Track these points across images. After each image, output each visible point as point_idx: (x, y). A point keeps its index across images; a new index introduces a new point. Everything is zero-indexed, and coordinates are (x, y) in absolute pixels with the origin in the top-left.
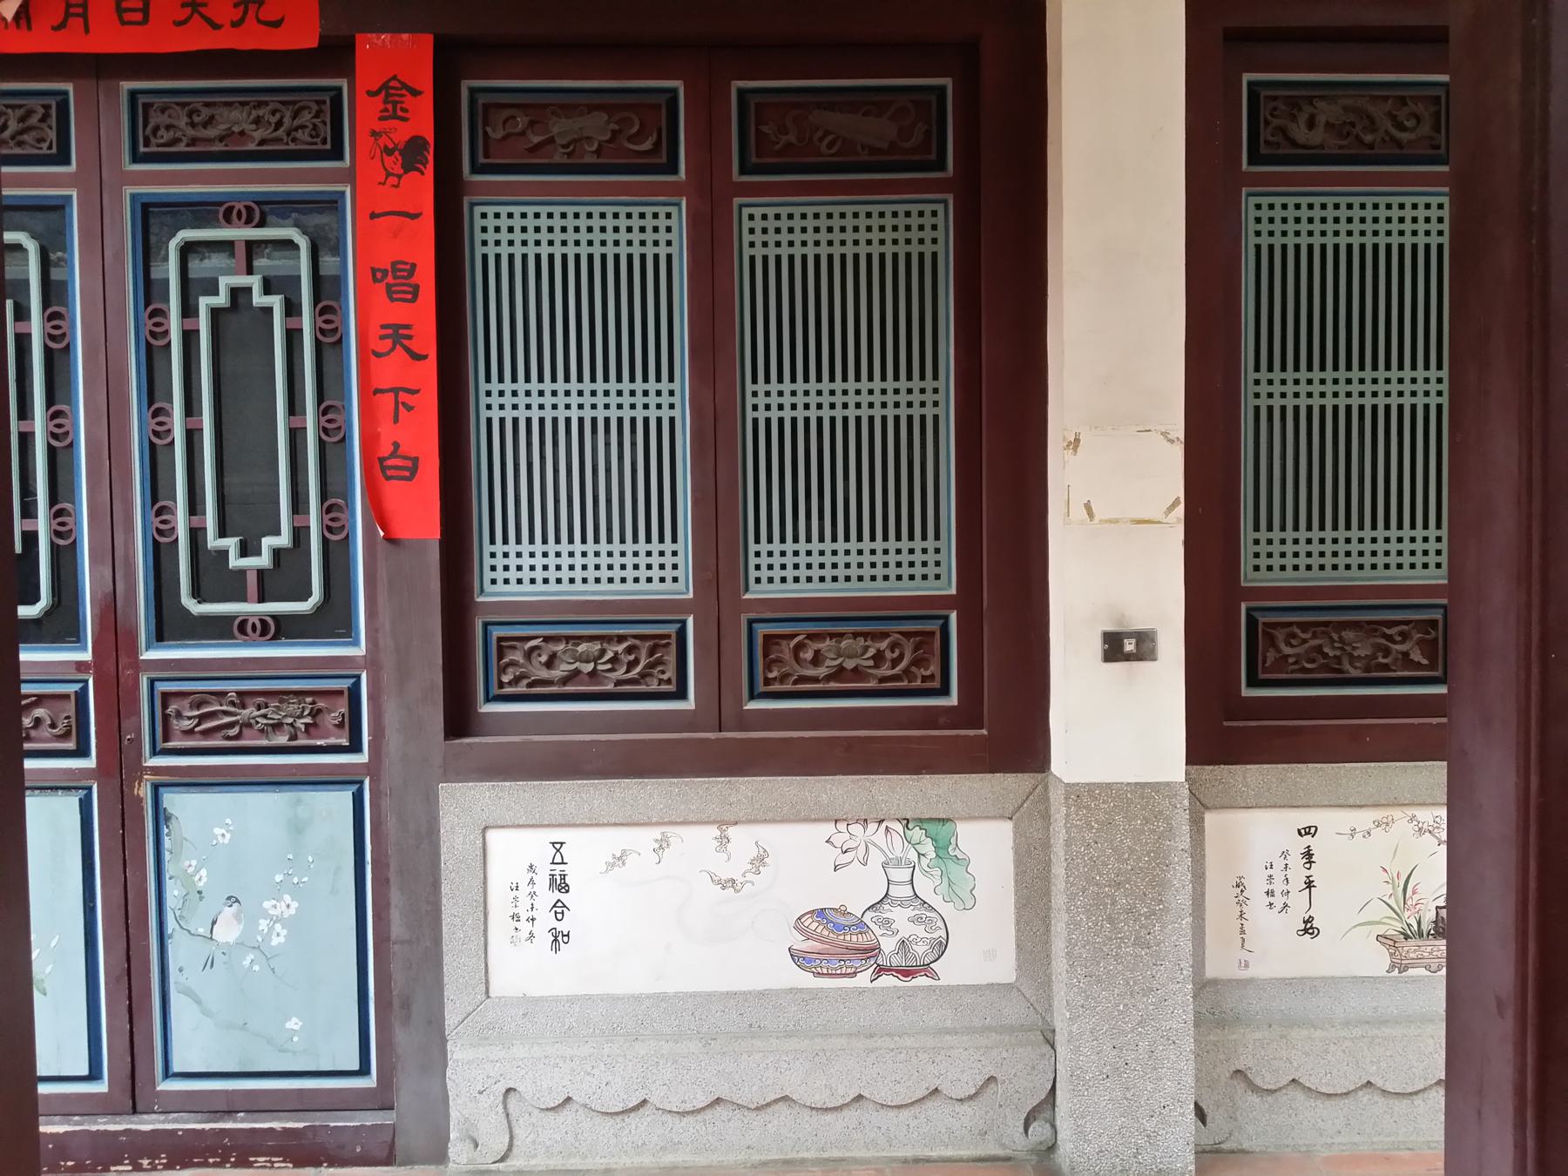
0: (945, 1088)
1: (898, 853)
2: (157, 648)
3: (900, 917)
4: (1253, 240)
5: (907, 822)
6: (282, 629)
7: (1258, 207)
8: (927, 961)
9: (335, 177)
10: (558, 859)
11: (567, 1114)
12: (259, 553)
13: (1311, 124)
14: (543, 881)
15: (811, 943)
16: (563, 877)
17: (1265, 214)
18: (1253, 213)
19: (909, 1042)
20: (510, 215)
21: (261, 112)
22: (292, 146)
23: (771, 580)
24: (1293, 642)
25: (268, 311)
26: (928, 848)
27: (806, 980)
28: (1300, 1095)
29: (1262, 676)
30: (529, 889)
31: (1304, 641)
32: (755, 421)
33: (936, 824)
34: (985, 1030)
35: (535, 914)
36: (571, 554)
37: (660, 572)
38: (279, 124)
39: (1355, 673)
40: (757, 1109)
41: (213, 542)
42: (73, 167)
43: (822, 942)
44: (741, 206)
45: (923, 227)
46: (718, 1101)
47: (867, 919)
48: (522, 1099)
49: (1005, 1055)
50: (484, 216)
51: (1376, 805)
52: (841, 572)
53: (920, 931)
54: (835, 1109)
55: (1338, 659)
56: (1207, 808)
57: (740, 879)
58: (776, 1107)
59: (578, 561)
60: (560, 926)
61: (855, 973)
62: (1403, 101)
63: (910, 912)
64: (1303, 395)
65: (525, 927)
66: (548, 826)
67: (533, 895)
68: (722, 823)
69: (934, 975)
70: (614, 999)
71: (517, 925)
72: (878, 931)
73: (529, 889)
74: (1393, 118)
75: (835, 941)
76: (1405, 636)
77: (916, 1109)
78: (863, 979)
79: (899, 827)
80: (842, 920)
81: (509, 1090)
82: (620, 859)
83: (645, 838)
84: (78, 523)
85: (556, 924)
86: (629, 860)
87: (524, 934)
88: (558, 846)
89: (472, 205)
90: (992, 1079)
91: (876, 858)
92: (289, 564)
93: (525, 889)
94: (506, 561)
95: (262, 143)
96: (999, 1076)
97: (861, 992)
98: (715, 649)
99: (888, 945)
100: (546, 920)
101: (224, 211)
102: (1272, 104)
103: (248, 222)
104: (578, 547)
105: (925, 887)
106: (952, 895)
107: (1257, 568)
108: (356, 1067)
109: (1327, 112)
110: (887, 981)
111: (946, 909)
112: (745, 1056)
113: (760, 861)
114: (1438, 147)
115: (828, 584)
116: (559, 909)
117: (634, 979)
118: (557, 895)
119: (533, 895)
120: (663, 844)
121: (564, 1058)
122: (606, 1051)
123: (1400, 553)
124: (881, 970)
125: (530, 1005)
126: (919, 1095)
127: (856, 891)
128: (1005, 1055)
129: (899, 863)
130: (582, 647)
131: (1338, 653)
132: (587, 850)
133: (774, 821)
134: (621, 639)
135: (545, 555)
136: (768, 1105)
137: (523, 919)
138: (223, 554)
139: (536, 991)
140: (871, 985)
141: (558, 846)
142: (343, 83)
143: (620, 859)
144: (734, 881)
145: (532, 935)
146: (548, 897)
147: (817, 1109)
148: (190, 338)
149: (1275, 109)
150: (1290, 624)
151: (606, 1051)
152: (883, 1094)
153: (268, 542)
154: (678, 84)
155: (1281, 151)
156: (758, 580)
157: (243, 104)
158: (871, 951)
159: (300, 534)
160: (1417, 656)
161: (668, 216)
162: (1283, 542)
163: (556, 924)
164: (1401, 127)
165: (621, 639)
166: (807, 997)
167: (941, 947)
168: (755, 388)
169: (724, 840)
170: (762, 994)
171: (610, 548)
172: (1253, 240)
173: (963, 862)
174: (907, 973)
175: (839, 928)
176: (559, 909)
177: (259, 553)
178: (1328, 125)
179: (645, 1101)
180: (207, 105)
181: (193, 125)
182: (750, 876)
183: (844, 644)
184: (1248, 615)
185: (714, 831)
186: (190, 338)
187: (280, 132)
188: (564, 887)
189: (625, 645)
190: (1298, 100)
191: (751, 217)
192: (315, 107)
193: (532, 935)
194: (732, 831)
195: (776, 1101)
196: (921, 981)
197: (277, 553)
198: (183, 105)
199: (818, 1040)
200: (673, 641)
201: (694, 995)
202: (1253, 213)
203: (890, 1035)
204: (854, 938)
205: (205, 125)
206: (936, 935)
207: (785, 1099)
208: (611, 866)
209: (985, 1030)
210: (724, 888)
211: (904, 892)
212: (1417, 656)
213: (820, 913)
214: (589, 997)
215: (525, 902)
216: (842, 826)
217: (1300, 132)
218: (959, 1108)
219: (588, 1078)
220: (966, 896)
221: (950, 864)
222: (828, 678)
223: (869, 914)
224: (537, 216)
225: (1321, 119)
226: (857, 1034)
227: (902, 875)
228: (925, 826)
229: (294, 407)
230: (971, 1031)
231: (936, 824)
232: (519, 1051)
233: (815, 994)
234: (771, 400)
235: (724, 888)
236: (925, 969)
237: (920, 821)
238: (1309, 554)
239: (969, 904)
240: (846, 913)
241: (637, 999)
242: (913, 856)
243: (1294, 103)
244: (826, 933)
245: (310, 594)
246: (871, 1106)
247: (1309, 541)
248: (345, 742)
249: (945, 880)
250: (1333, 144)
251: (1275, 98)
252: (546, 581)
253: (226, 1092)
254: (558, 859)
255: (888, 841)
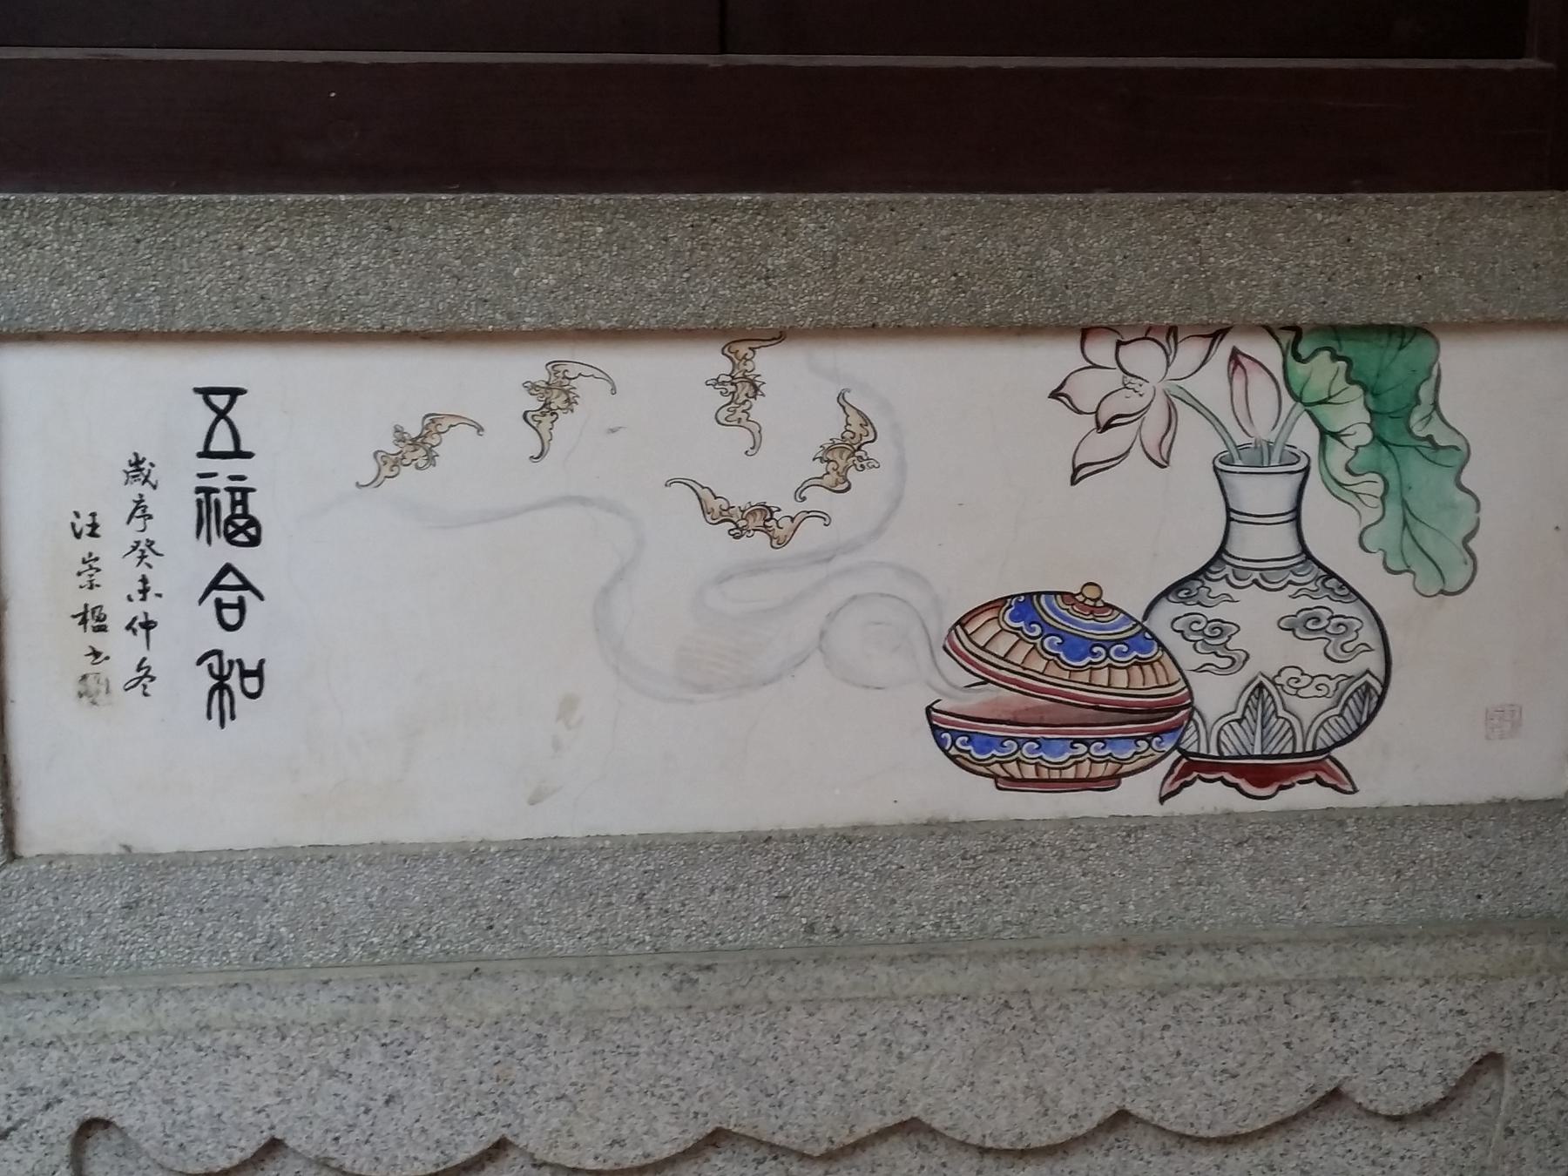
0: (1364, 1087)
1: (1263, 428)
3: (1255, 616)
5: (1292, 336)
8: (1324, 740)
10: (223, 442)
14: (174, 509)
15: (991, 693)
16: (241, 495)
19: (1264, 965)
26: (1352, 415)
27: (978, 799)
30: (131, 533)
33: (1378, 349)
34: (1478, 928)
35: (153, 608)
40: (829, 1157)
43: (1026, 690)
46: (716, 1139)
47: (1160, 623)
48: (128, 1147)
49: (1532, 994)
51: (193, 337)
53: (1310, 655)
54: (1051, 1151)
57: (788, 507)
58: (882, 1151)
60: (235, 646)
61: (1114, 780)
63: (1284, 604)
65: (123, 649)
67: (144, 550)
68: (740, 336)
69: (1341, 781)
70: (408, 858)
71: (98, 641)
72: (1189, 657)
73: (131, 533)
75: (1060, 683)
77: (1277, 1145)
78: (1138, 795)
79: (1268, 352)
80: (1087, 627)
81: (90, 1127)
82: (418, 445)
83: (496, 380)
85: (221, 640)
86: (452, 445)
87: (121, 668)
88: (221, 400)
90: (1492, 1061)
91: (1197, 445)
93: (118, 534)
96: (1514, 1056)
97: (1131, 828)
99: (1216, 696)
100: (188, 627)
105: (1333, 529)
106: (1410, 547)
110: (1206, 796)
111: (1388, 593)
112: (798, 1014)
113: (848, 452)
116: (230, 595)
117: (461, 798)
118: (223, 552)
119: (144, 550)
120: (552, 399)
121: (258, 1031)
122: (386, 1006)
124: (1192, 768)
125: (145, 880)
126: (1289, 1103)
127: (1133, 537)
128: (1532, 994)
129: (1259, 458)
132: (314, 410)
133: (898, 331)
136: (860, 1145)
137: (116, 622)
139: (164, 836)
140: (1157, 810)
141: (221, 400)
143: (418, 445)
144: (767, 511)
145: (144, 673)
146: (191, 559)
147: (998, 1153)
151: (386, 1006)
152: (1187, 1106)
158: (1165, 715)
163: (221, 640)
166: (974, 845)
167: (1367, 700)
169: (741, 389)
170: (848, 840)
173: (1450, 456)
174: (1264, 774)
175: (1078, 646)
176: (230, 595)
179: (501, 1147)
182: (818, 498)
185: (711, 361)
188: (244, 529)
193: (144, 673)
194: (768, 363)
195: (884, 1134)
196: (1306, 796)
199: (1010, 966)
201: (646, 845)
203: (1213, 947)
204: (1121, 678)
206: (1352, 668)
207: (910, 1127)
208: (390, 464)
209: (1478, 928)
210: (738, 533)
211: (1274, 543)
213: (1025, 606)
214: (325, 857)
215: (119, 575)
216: (1101, 350)
218: (1391, 1139)
219: (335, 1085)
220: (1448, 553)
221: (1416, 467)
223: (1169, 610)
226: (1122, 946)
227: (1264, 493)
228: (1348, 349)
230: (1437, 931)
231: (1378, 349)
232: (118, 1016)
233: (1002, 837)
235: (738, 533)
236: (1318, 764)
237: (1335, 334)
239: (1456, 579)
240: (1099, 608)
241: (474, 856)
242: (1305, 437)
244: (1039, 664)
246: (1149, 1140)
249: (1394, 509)
254: (223, 442)
255: (1230, 392)
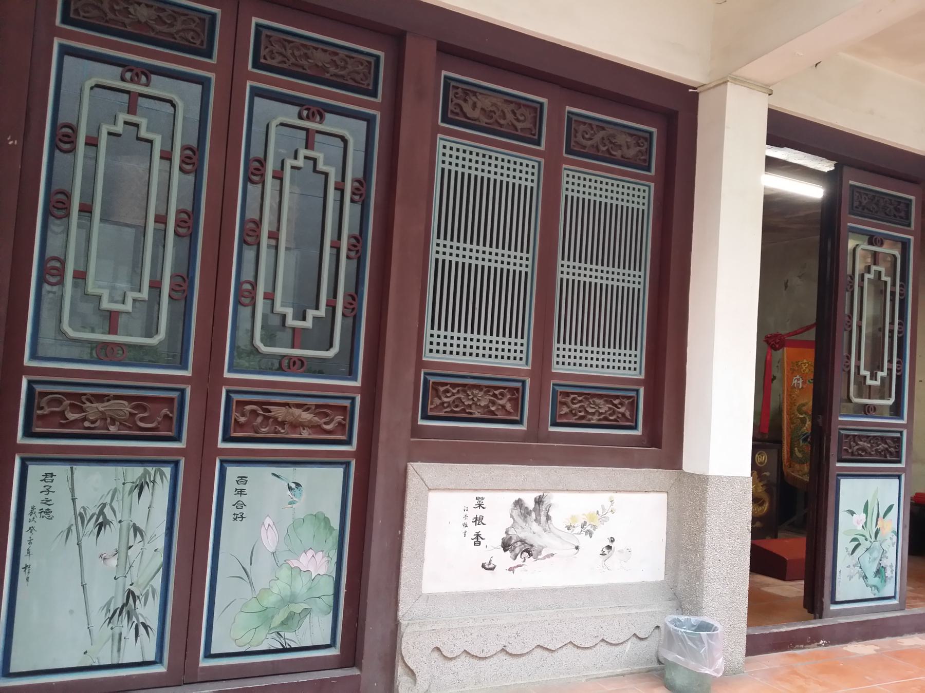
4: (441, 165)
7: (444, 147)
13: (474, 106)
17: (448, 152)
18: (442, 150)
20: (573, 177)
23: (451, 353)
24: (448, 395)
25: (886, 282)
28: (468, 659)
29: (430, 413)
31: (453, 394)
39: (477, 415)
42: (214, 61)
44: (649, 187)
45: (635, 195)
52: (493, 353)
54: (583, 648)
55: (470, 406)
56: (430, 490)
62: (519, 105)
66: (444, 489)
74: (515, 114)
76: (622, 404)
89: (649, 187)
102: (456, 91)
108: (328, 642)
109: (485, 102)
115: (627, 371)
131: (470, 403)
149: (457, 93)
150: (446, 384)
154: (544, 100)
155: (457, 118)
156: (558, 363)
160: (508, 406)
161: (533, 167)
164: (518, 120)
172: (441, 165)
178: (482, 109)
184: (425, 379)
190: (469, 91)
191: (568, 176)
202: (442, 150)
212: (508, 406)
217: (467, 108)
225: (479, 105)
243: (466, 92)
248: (344, 438)
250: (484, 121)
251: (458, 88)
253: (273, 662)
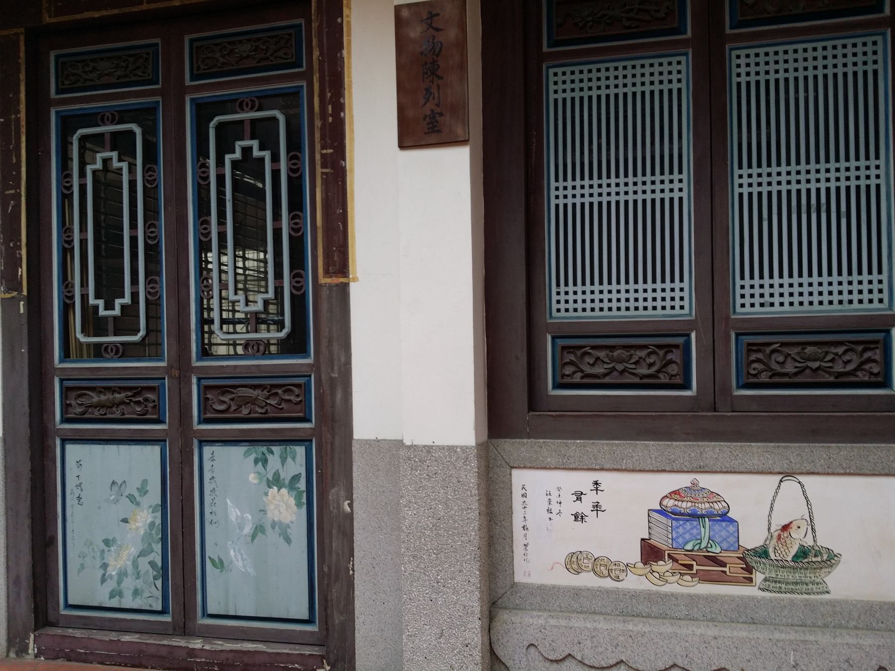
2: (66, 362)
6: (124, 352)
9: (153, 93)
11: (568, 663)
12: (113, 309)
21: (257, 44)
22: (133, 78)
25: (262, 160)
32: (557, 206)
36: (801, 285)
37: (672, 299)
38: (127, 68)
41: (92, 301)
50: (875, 43)
59: (623, 296)
64: (853, 168)
84: (161, 287)
92: (130, 311)
94: (567, 297)
95: (119, 78)
98: (712, 351)
101: (237, 104)
103: (252, 109)
104: (650, 286)
107: (559, 310)
114: (290, 35)
123: (601, 301)
130: (809, 350)
134: (841, 343)
135: (627, 291)
138: (96, 308)
142: (302, 21)
148: (221, 179)
153: (118, 302)
157: (249, 40)
159: (135, 296)
162: (601, 292)
165: (841, 343)
168: (741, 172)
171: (610, 287)
177: (113, 309)
180: (230, 43)
181: (85, 72)
183: (616, 353)
186: (221, 179)
187: (268, 54)
189: (845, 348)
192: (145, 56)
197: (123, 307)
198: (216, 45)
200: (880, 346)
205: (91, 72)
207: (557, 661)
222: (235, 387)
224: (805, 50)
229: (277, 216)
234: (744, 181)
238: (811, 294)
245: (139, 331)
247: (592, 292)
252: (831, 303)
